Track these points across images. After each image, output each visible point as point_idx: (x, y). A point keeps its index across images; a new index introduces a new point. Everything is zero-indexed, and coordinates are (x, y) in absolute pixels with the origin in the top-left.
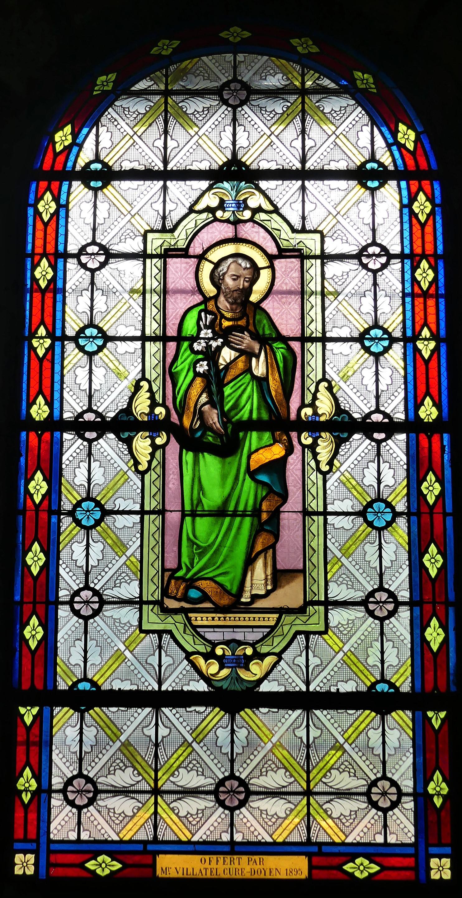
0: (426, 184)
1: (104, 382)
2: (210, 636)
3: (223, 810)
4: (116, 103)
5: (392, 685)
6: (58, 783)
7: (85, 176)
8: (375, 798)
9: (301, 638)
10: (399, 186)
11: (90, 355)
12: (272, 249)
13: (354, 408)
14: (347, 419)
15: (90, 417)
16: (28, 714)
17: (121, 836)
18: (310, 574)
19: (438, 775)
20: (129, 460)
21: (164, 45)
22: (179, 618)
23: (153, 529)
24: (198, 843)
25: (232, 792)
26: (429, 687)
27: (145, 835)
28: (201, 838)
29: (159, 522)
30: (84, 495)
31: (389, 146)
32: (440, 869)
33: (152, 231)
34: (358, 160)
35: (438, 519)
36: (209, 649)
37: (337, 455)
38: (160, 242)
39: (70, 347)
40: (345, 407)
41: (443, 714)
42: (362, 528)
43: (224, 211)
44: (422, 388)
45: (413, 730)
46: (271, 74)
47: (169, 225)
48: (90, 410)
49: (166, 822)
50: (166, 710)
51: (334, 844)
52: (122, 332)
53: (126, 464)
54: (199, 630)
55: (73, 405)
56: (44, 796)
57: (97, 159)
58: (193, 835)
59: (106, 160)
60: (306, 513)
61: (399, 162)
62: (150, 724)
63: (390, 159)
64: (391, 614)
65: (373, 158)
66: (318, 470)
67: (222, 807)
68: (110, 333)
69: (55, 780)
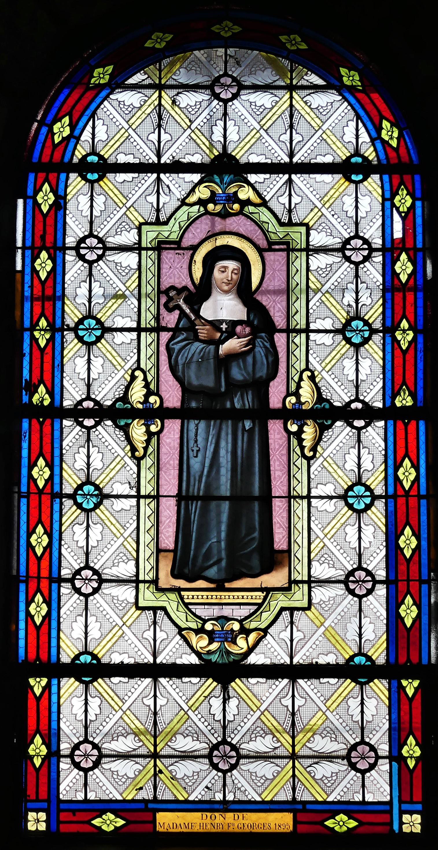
0: (407, 178)
1: (101, 372)
2: (200, 611)
3: (216, 772)
4: (111, 96)
5: (369, 658)
6: (66, 749)
7: (83, 168)
8: (215, 760)
9: (286, 614)
10: (381, 179)
11: (89, 345)
12: (263, 244)
13: (335, 397)
14: (327, 406)
15: (88, 404)
16: (38, 685)
17: (124, 795)
18: (295, 555)
19: (411, 740)
20: (126, 447)
21: (294, 39)
22: (173, 596)
23: (149, 512)
24: (333, 803)
25: (225, 757)
26: (402, 660)
27: (147, 794)
28: (197, 797)
29: (153, 505)
30: (84, 479)
31: (373, 141)
32: (412, 824)
33: (146, 223)
34: (343, 154)
35: (413, 501)
36: (200, 626)
37: (320, 442)
38: (154, 235)
39: (69, 336)
40: (326, 396)
41: (416, 683)
42: (343, 512)
43: (215, 205)
44: (399, 379)
45: (389, 699)
46: (260, 70)
47: (163, 217)
48: (88, 398)
49: (164, 784)
50: (300, 681)
51: (317, 802)
52: (119, 323)
53: (123, 449)
54: (190, 607)
55: (73, 394)
56: (54, 760)
57: (94, 152)
58: (328, 796)
59: (102, 153)
60: (157, 497)
61: (382, 156)
62: (287, 695)
63: (374, 154)
64: (370, 592)
65: (357, 153)
66: (304, 456)
67: (216, 770)
68: (107, 324)
69: (63, 746)
